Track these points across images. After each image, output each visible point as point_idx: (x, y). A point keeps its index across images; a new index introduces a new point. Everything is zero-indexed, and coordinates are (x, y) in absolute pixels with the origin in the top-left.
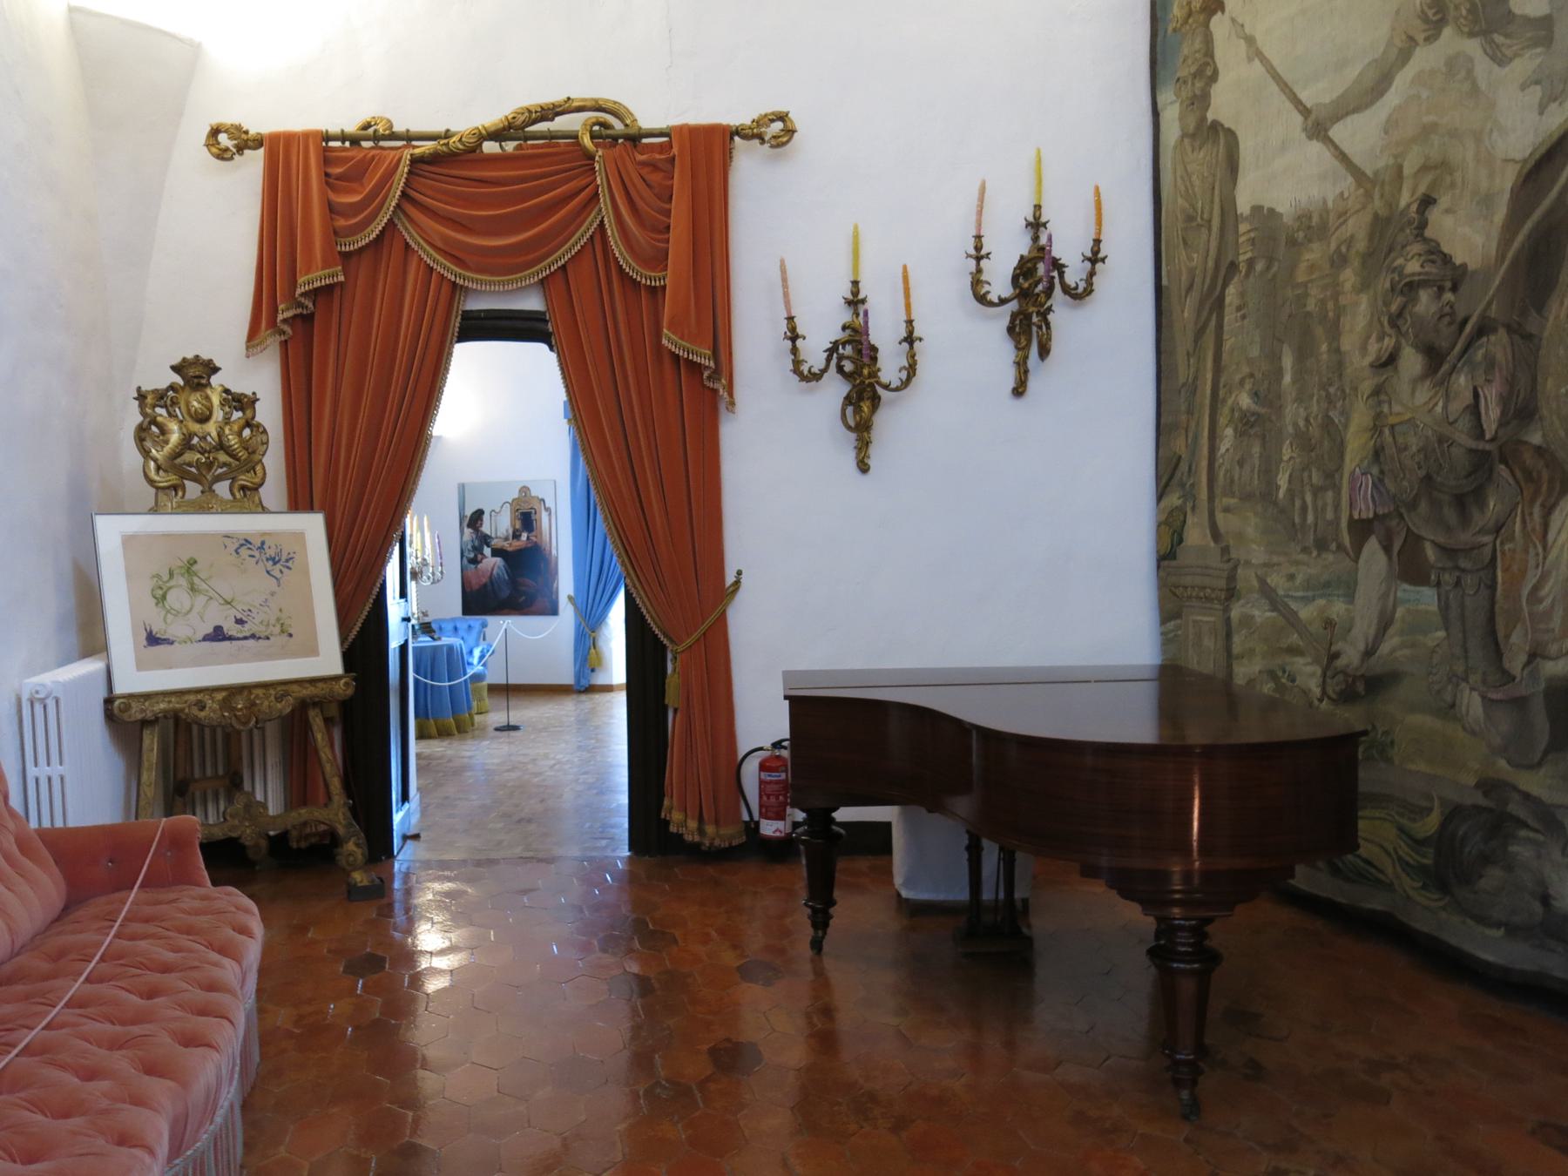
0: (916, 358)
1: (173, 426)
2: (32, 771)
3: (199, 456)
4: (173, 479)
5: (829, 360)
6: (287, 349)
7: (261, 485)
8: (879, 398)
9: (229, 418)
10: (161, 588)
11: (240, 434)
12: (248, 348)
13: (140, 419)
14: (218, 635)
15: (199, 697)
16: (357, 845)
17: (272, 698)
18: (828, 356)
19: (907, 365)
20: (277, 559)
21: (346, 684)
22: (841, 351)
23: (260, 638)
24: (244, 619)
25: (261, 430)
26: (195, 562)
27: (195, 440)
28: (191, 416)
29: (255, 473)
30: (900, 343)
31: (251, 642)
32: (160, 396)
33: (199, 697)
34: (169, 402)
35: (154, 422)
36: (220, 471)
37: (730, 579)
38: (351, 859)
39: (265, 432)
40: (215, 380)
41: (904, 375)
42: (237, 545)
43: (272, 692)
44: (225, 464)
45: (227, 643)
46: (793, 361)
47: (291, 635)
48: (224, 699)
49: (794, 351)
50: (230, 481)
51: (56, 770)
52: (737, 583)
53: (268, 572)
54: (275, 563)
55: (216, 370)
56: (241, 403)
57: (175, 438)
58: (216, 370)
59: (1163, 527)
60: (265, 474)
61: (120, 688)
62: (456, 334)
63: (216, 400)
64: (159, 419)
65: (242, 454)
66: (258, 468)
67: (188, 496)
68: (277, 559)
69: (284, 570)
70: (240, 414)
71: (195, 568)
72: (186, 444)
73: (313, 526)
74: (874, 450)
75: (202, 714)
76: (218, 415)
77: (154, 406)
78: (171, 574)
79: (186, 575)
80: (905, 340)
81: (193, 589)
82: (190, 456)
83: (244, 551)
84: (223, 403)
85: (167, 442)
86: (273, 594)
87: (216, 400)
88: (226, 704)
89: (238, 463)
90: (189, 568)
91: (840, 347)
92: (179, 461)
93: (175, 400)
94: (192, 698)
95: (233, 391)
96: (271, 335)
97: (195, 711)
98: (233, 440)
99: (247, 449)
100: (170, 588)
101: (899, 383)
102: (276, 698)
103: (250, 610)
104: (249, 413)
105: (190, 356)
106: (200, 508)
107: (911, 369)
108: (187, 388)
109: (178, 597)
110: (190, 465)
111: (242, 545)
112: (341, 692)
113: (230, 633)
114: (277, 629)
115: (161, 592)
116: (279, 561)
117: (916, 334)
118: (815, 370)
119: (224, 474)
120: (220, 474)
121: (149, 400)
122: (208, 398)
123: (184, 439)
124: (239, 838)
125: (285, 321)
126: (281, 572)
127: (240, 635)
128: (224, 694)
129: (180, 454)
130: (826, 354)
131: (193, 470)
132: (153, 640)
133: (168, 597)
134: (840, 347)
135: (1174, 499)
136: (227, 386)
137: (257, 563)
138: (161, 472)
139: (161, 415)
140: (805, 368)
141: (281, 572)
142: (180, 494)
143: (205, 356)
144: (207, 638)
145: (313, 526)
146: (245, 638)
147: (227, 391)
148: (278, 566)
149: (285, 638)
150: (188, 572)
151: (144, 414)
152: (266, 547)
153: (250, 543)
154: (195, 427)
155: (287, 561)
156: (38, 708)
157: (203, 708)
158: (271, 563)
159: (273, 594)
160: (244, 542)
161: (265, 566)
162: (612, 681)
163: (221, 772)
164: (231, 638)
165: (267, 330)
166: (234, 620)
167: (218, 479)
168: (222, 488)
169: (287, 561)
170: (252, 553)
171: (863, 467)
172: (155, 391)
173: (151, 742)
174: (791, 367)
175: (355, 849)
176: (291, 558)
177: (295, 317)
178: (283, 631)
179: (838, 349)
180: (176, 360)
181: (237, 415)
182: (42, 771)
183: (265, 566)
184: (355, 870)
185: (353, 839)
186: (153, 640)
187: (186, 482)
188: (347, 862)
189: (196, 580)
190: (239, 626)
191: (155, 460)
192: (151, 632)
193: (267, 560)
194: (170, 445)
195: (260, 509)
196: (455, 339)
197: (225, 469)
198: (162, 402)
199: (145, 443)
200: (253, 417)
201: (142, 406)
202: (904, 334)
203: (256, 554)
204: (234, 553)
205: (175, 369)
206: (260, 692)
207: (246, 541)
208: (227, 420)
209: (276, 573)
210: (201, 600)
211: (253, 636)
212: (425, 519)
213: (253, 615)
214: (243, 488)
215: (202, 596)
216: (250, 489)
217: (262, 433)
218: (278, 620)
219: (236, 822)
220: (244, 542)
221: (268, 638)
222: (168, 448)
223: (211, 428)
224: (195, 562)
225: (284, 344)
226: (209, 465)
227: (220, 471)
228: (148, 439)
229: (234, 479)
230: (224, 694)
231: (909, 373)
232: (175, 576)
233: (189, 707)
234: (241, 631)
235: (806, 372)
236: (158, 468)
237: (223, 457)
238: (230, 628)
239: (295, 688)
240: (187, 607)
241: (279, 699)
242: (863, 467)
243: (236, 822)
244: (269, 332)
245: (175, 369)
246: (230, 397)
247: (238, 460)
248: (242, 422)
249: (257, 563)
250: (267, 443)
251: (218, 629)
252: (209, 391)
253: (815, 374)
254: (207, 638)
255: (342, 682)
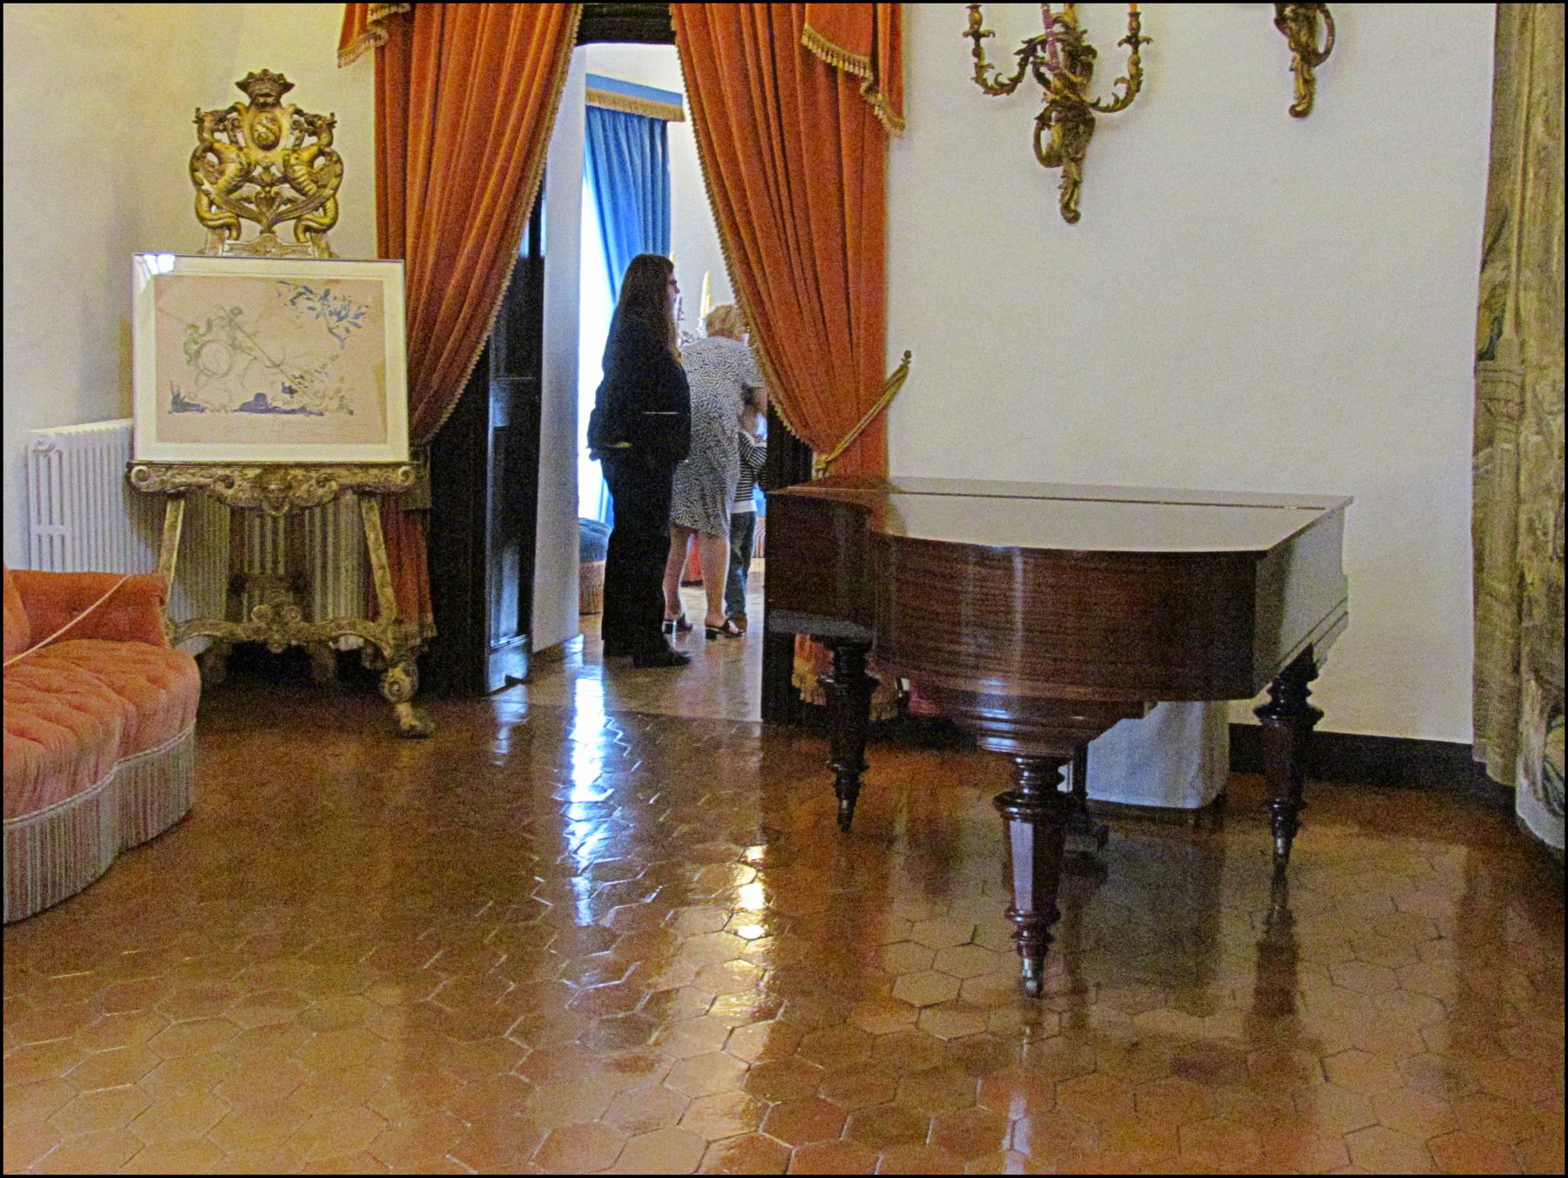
0: (1141, 66)
1: (231, 153)
2: (35, 529)
3: (258, 188)
4: (227, 216)
5: (1023, 65)
6: (383, 55)
7: (330, 226)
8: (1093, 120)
9: (299, 145)
10: (196, 343)
11: (311, 163)
12: (340, 56)
13: (197, 143)
14: (259, 404)
15: (228, 472)
16: (407, 673)
17: (313, 482)
18: (1022, 59)
19: (1128, 77)
20: (343, 314)
21: (406, 474)
22: (1040, 53)
23: (311, 413)
24: (294, 387)
25: (335, 159)
26: (241, 312)
27: (259, 170)
28: (253, 141)
29: (325, 210)
30: (1120, 44)
31: (300, 416)
32: (220, 119)
33: (228, 472)
34: (229, 126)
35: (211, 149)
36: (283, 208)
37: (892, 365)
38: (396, 687)
39: (339, 161)
40: (286, 99)
41: (1121, 91)
42: (293, 294)
43: (313, 474)
44: (289, 201)
45: (269, 416)
46: (976, 65)
47: (351, 413)
48: (256, 476)
49: (977, 52)
50: (294, 221)
51: (57, 529)
52: (903, 371)
53: (330, 330)
54: (340, 319)
55: (288, 87)
56: (315, 126)
57: (232, 169)
58: (288, 87)
59: (1483, 310)
60: (337, 213)
61: (140, 456)
62: (575, 35)
63: (286, 123)
64: (217, 145)
65: (311, 188)
66: (330, 205)
67: (244, 236)
68: (343, 314)
69: (352, 328)
70: (314, 139)
71: (240, 318)
72: (246, 175)
73: (393, 274)
74: (1085, 190)
75: (230, 492)
76: (287, 140)
77: (212, 132)
78: (209, 326)
79: (228, 329)
80: (1128, 40)
81: (235, 346)
82: (249, 189)
83: (303, 303)
84: (296, 125)
85: (222, 173)
86: (334, 358)
87: (286, 123)
88: (259, 483)
89: (303, 198)
90: (231, 320)
91: (1039, 48)
92: (236, 195)
93: (236, 123)
94: (220, 472)
95: (305, 111)
96: (364, 40)
97: (220, 487)
98: (300, 171)
99: (316, 183)
100: (204, 345)
101: (1111, 101)
102: (318, 482)
103: (302, 377)
104: (325, 138)
105: (257, 71)
106: (255, 251)
107: (1135, 81)
108: (253, 109)
109: (215, 354)
110: (248, 200)
111: (300, 294)
112: (399, 482)
113: (274, 404)
114: (335, 404)
115: (195, 347)
116: (346, 316)
117: (1142, 34)
118: (1004, 80)
119: (288, 212)
120: (283, 212)
121: (208, 124)
122: (274, 120)
123: (241, 170)
124: (265, 643)
125: (377, 23)
126: (348, 330)
127: (284, 407)
128: (258, 471)
129: (237, 187)
130: (1017, 59)
131: (252, 206)
132: (180, 405)
133: (205, 351)
134: (1039, 48)
135: (1496, 272)
136: (300, 106)
137: (317, 317)
138: (214, 208)
139: (219, 141)
140: (989, 77)
141: (348, 330)
142: (234, 234)
143: (274, 71)
144: (245, 408)
145: (393, 274)
146: (293, 411)
147: (298, 112)
148: (345, 323)
149: (343, 415)
150: (230, 325)
151: (202, 140)
152: (330, 297)
153: (311, 292)
154: (257, 154)
155: (357, 317)
156: (43, 462)
157: (230, 485)
158: (335, 318)
159: (334, 358)
160: (303, 290)
161: (327, 322)
162: (903, 527)
163: (281, 571)
164: (274, 410)
165: (359, 33)
166: (280, 388)
167: (279, 218)
168: (284, 229)
169: (357, 317)
170: (311, 304)
171: (1071, 215)
172: (213, 113)
173: (174, 515)
174: (973, 74)
175: (403, 677)
176: (363, 314)
177: (390, 16)
178: (341, 407)
179: (1035, 50)
180: (242, 77)
181: (309, 140)
182: (45, 530)
183: (327, 322)
184: (400, 701)
185: (401, 665)
186: (180, 405)
187: (242, 220)
188: (390, 691)
189: (239, 335)
190: (287, 396)
191: (207, 194)
192: (178, 395)
193: (331, 314)
194: (225, 177)
195: (326, 256)
196: (575, 41)
197: (289, 206)
198: (221, 127)
199: (197, 174)
200: (330, 144)
201: (201, 130)
202: (1126, 33)
203: (318, 305)
204: (289, 303)
205: (243, 86)
206: (299, 473)
207: (305, 288)
208: (296, 148)
209: (340, 331)
210: (243, 360)
211: (302, 410)
212: (706, 276)
213: (306, 384)
214: (308, 229)
215: (244, 356)
216: (317, 231)
217: (336, 162)
218: (338, 391)
219: (263, 625)
220: (303, 290)
221: (322, 414)
222: (222, 182)
223: (276, 155)
224: (241, 312)
225: (381, 51)
226: (270, 201)
227: (283, 208)
228: (201, 169)
229: (299, 218)
230: (258, 471)
231: (1129, 88)
232: (214, 329)
233: (215, 482)
234: (288, 403)
235: (990, 82)
236: (211, 203)
237: (287, 191)
238: (278, 399)
239: (343, 472)
240: (225, 367)
241: (321, 483)
242: (1071, 215)
243: (263, 625)
244: (361, 37)
245: (243, 86)
246: (302, 119)
247: (304, 195)
248: (314, 150)
249: (317, 317)
250: (340, 176)
251: (260, 396)
252: (277, 112)
253: (1002, 85)
254: (245, 408)
255: (404, 468)
